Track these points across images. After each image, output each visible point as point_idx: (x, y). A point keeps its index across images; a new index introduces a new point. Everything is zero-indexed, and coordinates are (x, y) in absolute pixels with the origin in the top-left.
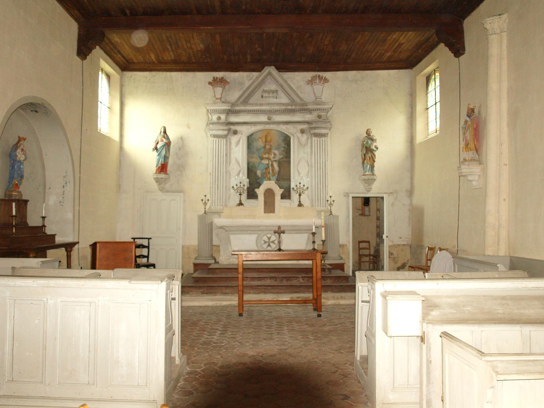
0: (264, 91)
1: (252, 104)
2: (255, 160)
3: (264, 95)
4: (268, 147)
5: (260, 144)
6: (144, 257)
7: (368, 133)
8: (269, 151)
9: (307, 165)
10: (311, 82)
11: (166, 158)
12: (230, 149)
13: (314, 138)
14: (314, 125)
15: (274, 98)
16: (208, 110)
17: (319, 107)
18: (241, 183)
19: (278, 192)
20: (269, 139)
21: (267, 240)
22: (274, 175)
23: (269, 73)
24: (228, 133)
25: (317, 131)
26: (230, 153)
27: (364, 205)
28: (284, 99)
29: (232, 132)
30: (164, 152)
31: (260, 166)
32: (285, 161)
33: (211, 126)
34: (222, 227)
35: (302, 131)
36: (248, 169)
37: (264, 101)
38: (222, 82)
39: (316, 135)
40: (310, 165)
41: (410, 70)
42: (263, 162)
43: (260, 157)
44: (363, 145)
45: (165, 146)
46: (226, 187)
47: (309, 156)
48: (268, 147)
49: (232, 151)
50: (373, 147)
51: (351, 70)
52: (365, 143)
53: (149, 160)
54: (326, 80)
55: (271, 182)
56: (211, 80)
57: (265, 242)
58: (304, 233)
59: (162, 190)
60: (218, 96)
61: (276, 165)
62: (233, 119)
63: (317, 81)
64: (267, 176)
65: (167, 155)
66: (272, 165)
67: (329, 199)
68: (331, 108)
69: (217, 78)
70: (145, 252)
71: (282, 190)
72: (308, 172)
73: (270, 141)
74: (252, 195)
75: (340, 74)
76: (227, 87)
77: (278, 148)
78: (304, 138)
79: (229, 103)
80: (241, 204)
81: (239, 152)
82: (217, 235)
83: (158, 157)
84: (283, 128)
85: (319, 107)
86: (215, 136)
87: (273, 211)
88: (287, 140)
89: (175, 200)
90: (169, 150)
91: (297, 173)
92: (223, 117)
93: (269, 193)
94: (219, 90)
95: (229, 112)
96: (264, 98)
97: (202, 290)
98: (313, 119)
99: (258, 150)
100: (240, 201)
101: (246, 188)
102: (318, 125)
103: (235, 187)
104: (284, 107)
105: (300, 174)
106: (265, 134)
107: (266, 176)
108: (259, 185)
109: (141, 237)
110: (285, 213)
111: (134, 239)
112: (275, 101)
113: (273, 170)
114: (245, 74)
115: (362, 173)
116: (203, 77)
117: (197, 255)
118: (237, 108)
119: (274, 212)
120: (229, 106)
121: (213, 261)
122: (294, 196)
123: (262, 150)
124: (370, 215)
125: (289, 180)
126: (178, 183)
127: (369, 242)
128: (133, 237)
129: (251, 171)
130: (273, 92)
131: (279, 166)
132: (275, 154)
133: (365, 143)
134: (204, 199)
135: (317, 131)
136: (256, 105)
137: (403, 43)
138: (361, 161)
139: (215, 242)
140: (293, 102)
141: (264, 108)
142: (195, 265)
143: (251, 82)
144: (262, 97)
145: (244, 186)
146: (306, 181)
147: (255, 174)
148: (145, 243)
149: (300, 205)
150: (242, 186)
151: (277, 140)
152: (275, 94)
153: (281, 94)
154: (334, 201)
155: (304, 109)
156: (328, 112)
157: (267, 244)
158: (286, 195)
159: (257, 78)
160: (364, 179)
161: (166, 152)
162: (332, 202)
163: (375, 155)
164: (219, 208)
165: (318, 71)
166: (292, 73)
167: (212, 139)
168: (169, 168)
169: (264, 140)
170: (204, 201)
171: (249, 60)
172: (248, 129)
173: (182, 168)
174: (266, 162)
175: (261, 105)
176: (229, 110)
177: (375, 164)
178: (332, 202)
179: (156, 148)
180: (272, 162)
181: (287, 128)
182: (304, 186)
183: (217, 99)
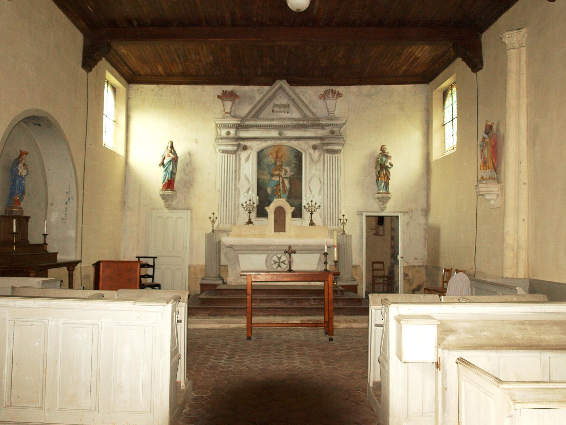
0: (276, 106)
1: (263, 119)
2: (266, 177)
5: (270, 160)
6: (149, 276)
7: (383, 149)
8: (280, 168)
9: (319, 182)
10: (323, 97)
11: (173, 174)
13: (326, 155)
14: (326, 141)
15: (285, 112)
17: (332, 122)
19: (289, 210)
20: (280, 155)
21: (277, 260)
22: (284, 193)
23: (281, 87)
24: (238, 149)
25: (330, 147)
28: (296, 114)
30: (171, 168)
31: (270, 183)
33: (220, 141)
34: (230, 247)
35: (315, 148)
37: (275, 116)
39: (329, 151)
41: (426, 85)
44: (377, 162)
46: (235, 204)
47: (321, 173)
48: (278, 163)
49: (242, 167)
52: (379, 160)
53: (155, 176)
54: (339, 95)
56: (220, 93)
57: (275, 262)
60: (228, 110)
61: (286, 182)
62: (243, 134)
63: (330, 95)
64: (277, 194)
65: (174, 171)
66: (283, 182)
67: (342, 218)
68: (344, 124)
69: (226, 91)
70: (150, 271)
71: (293, 208)
73: (281, 158)
74: (262, 213)
75: (354, 88)
76: (237, 101)
77: (289, 164)
79: (238, 117)
80: (250, 222)
81: (249, 168)
82: (226, 254)
83: (164, 173)
84: (294, 144)
85: (332, 122)
88: (298, 156)
89: (181, 217)
90: (176, 166)
91: (308, 190)
92: (232, 132)
93: (280, 212)
94: (228, 104)
95: (238, 127)
96: (275, 113)
97: (209, 312)
98: (326, 134)
99: (269, 166)
100: (250, 219)
101: (255, 205)
102: (330, 140)
103: (245, 205)
104: (295, 122)
105: (311, 193)
106: (276, 149)
107: (276, 194)
108: (269, 203)
111: (139, 258)
112: (286, 115)
114: (256, 88)
118: (247, 123)
120: (238, 121)
121: (221, 282)
122: (306, 214)
123: (273, 167)
125: (301, 198)
127: (383, 263)
128: (138, 256)
129: (261, 188)
132: (286, 171)
133: (379, 160)
134: (212, 217)
135: (330, 147)
136: (267, 120)
138: (375, 178)
139: (223, 261)
140: (305, 117)
141: (274, 123)
143: (261, 96)
144: (273, 112)
145: (254, 203)
148: (150, 262)
149: (312, 224)
150: (252, 204)
151: (288, 156)
152: (286, 109)
153: (293, 108)
154: (346, 220)
155: (315, 123)
156: (341, 128)
157: (277, 264)
158: (297, 214)
159: (268, 92)
161: (173, 168)
162: (345, 221)
163: (389, 173)
165: (331, 85)
167: (221, 154)
169: (274, 155)
170: (212, 219)
171: (260, 73)
173: (189, 184)
175: (272, 120)
176: (239, 124)
178: (345, 221)
179: (163, 164)
180: (282, 178)
181: (298, 144)
182: (316, 204)
183: (226, 113)
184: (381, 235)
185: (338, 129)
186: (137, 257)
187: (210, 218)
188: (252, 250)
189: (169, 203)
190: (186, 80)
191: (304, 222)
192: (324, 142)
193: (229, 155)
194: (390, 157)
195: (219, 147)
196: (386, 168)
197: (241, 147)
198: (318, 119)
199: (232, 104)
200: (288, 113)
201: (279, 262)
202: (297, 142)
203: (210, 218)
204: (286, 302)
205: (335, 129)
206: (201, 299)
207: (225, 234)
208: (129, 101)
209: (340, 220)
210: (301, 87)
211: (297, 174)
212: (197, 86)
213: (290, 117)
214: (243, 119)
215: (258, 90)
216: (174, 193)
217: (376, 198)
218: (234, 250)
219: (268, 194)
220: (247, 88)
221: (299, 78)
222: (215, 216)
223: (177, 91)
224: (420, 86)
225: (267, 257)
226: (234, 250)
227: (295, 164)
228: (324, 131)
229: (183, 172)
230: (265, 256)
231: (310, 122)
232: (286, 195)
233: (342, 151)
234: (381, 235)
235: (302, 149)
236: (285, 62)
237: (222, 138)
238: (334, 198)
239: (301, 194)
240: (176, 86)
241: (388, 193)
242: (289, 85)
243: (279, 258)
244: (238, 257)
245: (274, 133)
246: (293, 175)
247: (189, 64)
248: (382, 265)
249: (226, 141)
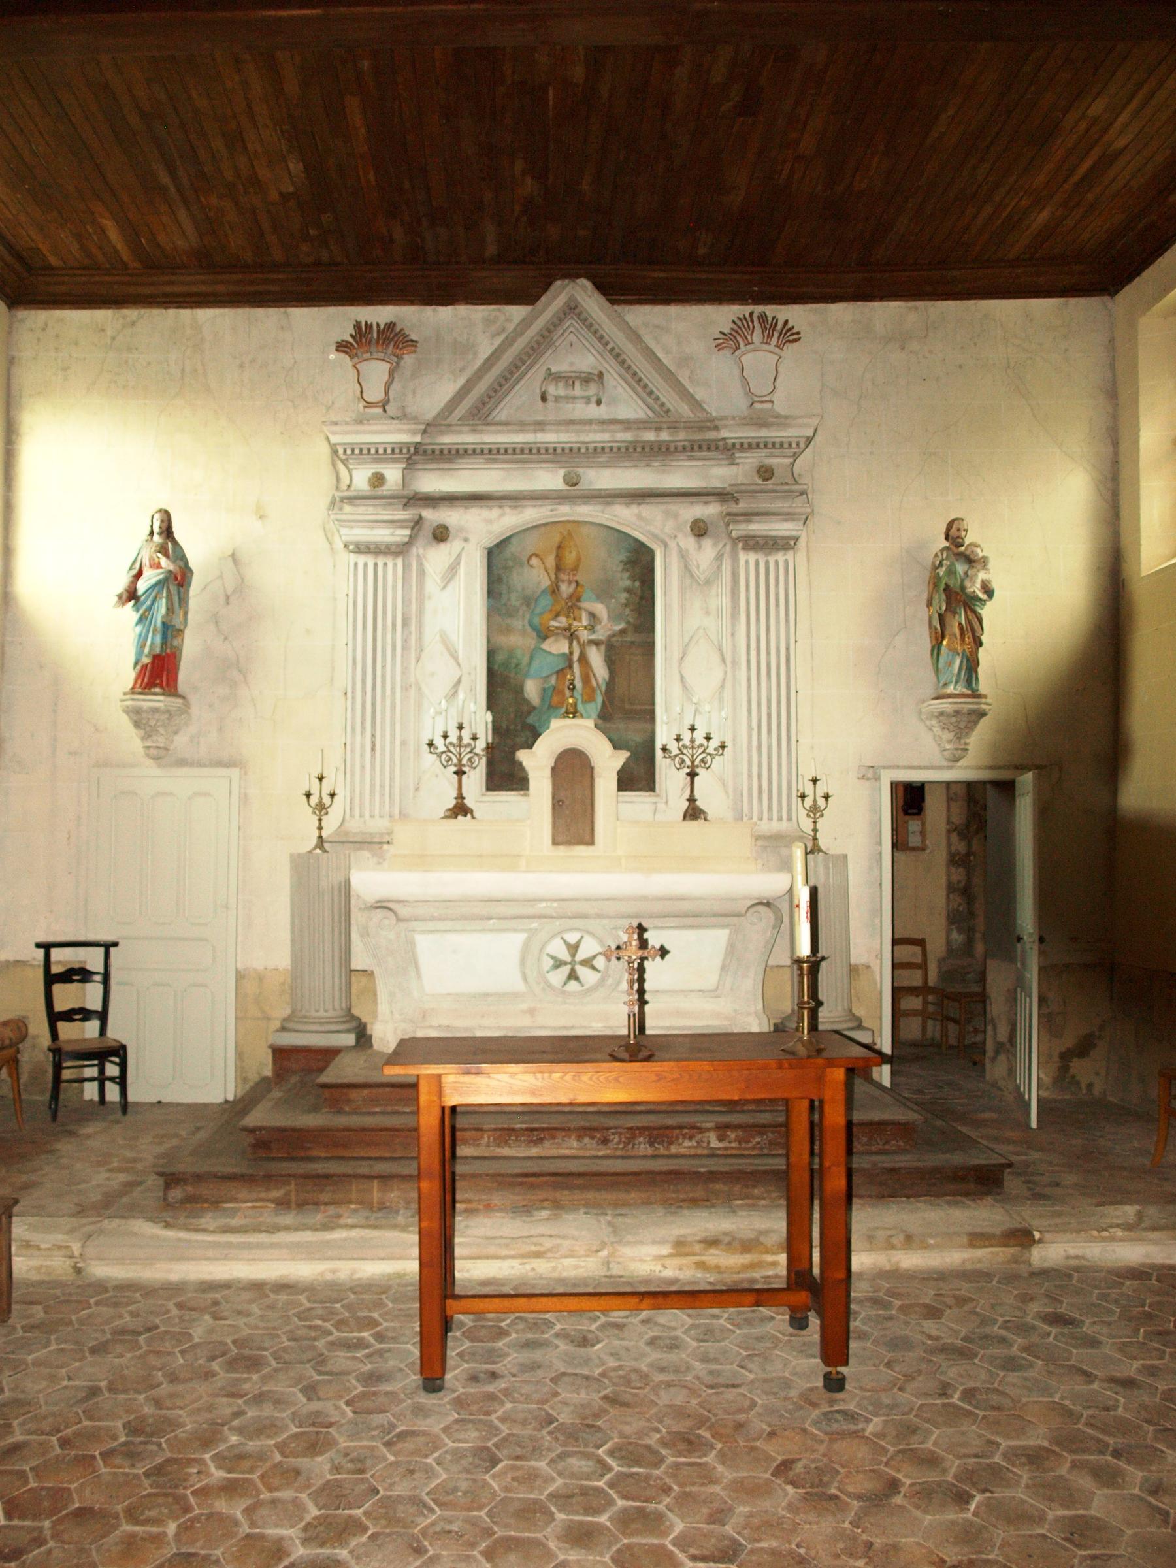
0: (556, 378)
1: (506, 424)
2: (519, 641)
3: (552, 390)
4: (566, 589)
5: (536, 577)
6: (85, 1014)
7: (953, 534)
8: (572, 605)
9: (716, 658)
10: (732, 340)
11: (171, 631)
12: (421, 599)
13: (743, 556)
14: (742, 506)
15: (588, 400)
16: (335, 452)
17: (764, 433)
18: (460, 728)
19: (608, 761)
20: (570, 557)
21: (564, 955)
22: (589, 698)
23: (572, 309)
24: (412, 539)
25: (757, 527)
26: (421, 611)
27: (906, 813)
28: (629, 407)
29: (427, 531)
30: (163, 610)
31: (535, 665)
32: (635, 646)
33: (347, 508)
34: (382, 906)
35: (700, 530)
36: (491, 673)
37: (551, 412)
38: (392, 340)
39: (753, 543)
40: (729, 660)
41: (1106, 298)
42: (546, 646)
43: (534, 629)
44: (935, 581)
45: (166, 584)
46: (404, 743)
47: (726, 619)
48: (566, 589)
49: (429, 606)
50: (975, 588)
51: (882, 298)
52: (942, 571)
53: (101, 641)
54: (789, 335)
55: (578, 721)
56: (346, 333)
57: (558, 964)
58: (715, 926)
59: (160, 756)
60: (375, 393)
61: (596, 659)
62: (432, 482)
63: (757, 336)
64: (562, 702)
65: (177, 621)
66: (583, 659)
67: (809, 789)
68: (809, 440)
69: (369, 326)
70: (91, 996)
71: (622, 756)
72: (722, 686)
73: (575, 569)
74: (505, 775)
75: (841, 312)
76: (408, 360)
77: (604, 593)
78: (705, 554)
79: (415, 419)
80: (461, 809)
81: (453, 609)
82: (365, 933)
83: (139, 629)
84: (624, 517)
85: (764, 433)
86: (362, 549)
87: (588, 839)
88: (640, 562)
89: (206, 794)
90: (184, 601)
91: (677, 689)
92: (393, 474)
93: (572, 769)
94: (376, 370)
95: (416, 456)
96: (550, 404)
97: (276, 1194)
98: (740, 480)
99: (528, 601)
100: (460, 797)
101: (481, 745)
102: (758, 508)
103: (439, 743)
104: (628, 436)
105: (691, 688)
106: (557, 539)
107: (559, 702)
108: (531, 735)
109: (82, 938)
110: (636, 854)
111: (47, 947)
112: (593, 411)
113: (586, 680)
114: (479, 312)
115: (930, 691)
116: (321, 326)
117: (288, 1011)
118: (448, 439)
119: (591, 842)
120: (414, 433)
121: (349, 1039)
122: (670, 776)
123: (546, 602)
124: (923, 849)
125: (650, 715)
126: (220, 729)
127: (921, 943)
128: (43, 938)
129: (501, 683)
130: (586, 380)
131: (610, 662)
132: (592, 615)
133: (942, 571)
134: (315, 791)
135: (757, 527)
136: (522, 426)
137: (1119, 154)
138: (926, 643)
139: (359, 961)
140: (663, 417)
141: (549, 437)
142: (280, 1054)
143: (498, 341)
144: (544, 399)
145: (475, 738)
146: (714, 720)
147: (519, 690)
148: (93, 960)
149: (693, 812)
150: (466, 740)
151: (603, 562)
152: (592, 389)
153: (615, 384)
154: (826, 797)
155: (704, 442)
156: (796, 456)
157: (566, 970)
158: (638, 777)
159: (526, 323)
160: (942, 714)
161: (170, 610)
162: (821, 802)
163: (980, 620)
164: (377, 825)
165: (759, 299)
166: (659, 309)
167: (353, 557)
168: (186, 674)
169: (551, 561)
170: (314, 800)
171: (491, 250)
172: (489, 522)
173: (233, 671)
174: (559, 646)
175: (540, 426)
176: (417, 446)
177: (982, 653)
178: (821, 802)
179: (131, 595)
180: (582, 646)
181: (639, 517)
182: (708, 738)
183: (369, 405)
184: (914, 849)
185: (788, 461)
186: (38, 945)
187: (308, 795)
188: (465, 918)
189: (161, 741)
190: (221, 288)
191: (661, 806)
192: (734, 508)
193: (381, 561)
194: (984, 561)
195: (344, 531)
196: (970, 604)
197: (427, 531)
198: (712, 424)
199: (392, 373)
200: (599, 403)
201: (573, 963)
202: (634, 509)
203: (308, 795)
204: (605, 1141)
205: (773, 461)
206: (251, 1131)
207: (366, 854)
208: (15, 370)
209: (803, 797)
210: (647, 309)
211: (637, 629)
212: (259, 312)
213: (605, 417)
214: (429, 427)
215: (488, 322)
216: (175, 702)
217: (932, 716)
218: (398, 919)
219: (527, 702)
220: (444, 314)
221: (641, 270)
222: (327, 787)
223: (189, 332)
224: (1082, 301)
225: (526, 947)
226: (399, 919)
227: (628, 590)
228: (734, 468)
229: (212, 627)
230: (522, 936)
231: (682, 435)
232: (595, 707)
233: (802, 542)
234: (914, 849)
235: (655, 536)
236: (586, 186)
237: (353, 499)
238: (777, 718)
239: (652, 702)
240: (186, 314)
241: (975, 695)
242: (602, 299)
243: (573, 948)
244: (412, 944)
245: (550, 479)
246: (623, 632)
247: (214, 200)
248: (918, 949)
249: (371, 510)
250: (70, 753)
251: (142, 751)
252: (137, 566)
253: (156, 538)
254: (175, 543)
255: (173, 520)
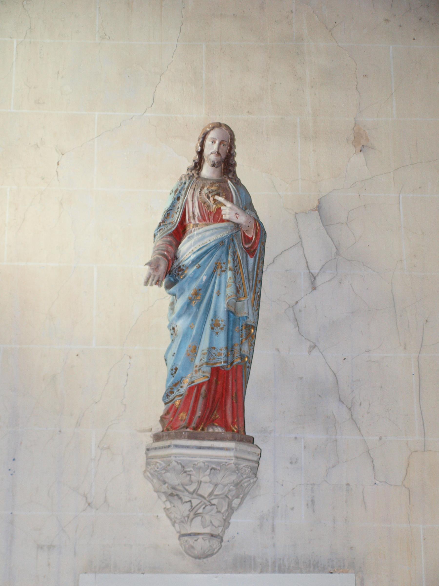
11: (242, 330)
168: (258, 406)
250: (40, 547)
251: (174, 542)
252: (176, 218)
253: (207, 171)
254: (237, 182)
255: (237, 143)
